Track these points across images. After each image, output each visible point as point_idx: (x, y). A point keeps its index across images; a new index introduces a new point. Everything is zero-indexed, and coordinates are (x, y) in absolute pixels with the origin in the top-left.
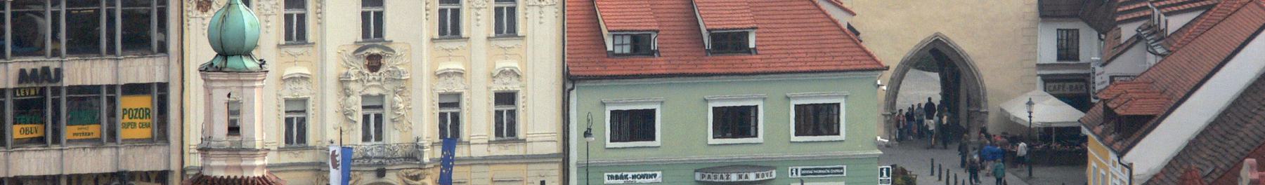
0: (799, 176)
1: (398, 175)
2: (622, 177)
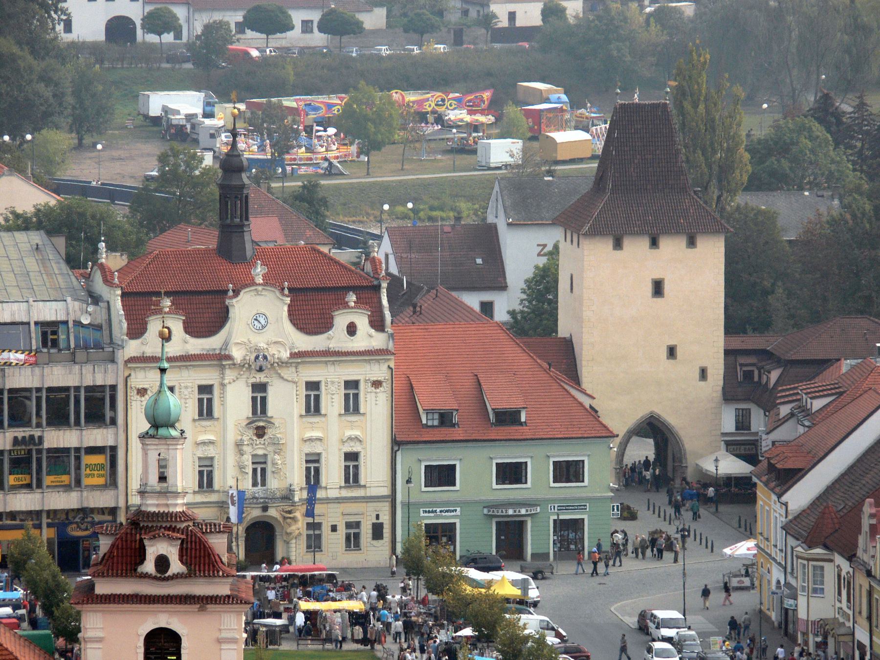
0: (556, 511)
1: (277, 510)
2: (432, 512)
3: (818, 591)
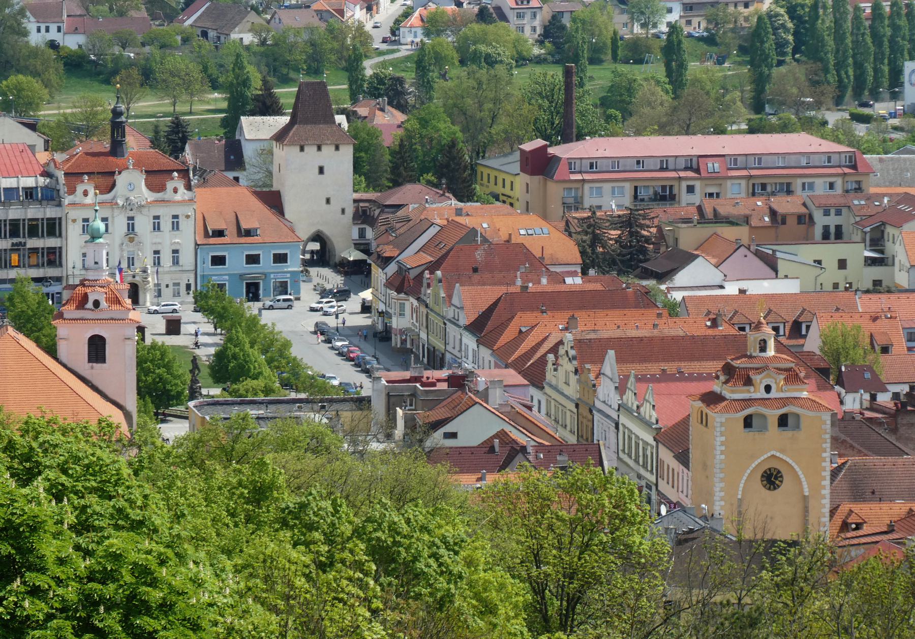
3: (402, 315)
